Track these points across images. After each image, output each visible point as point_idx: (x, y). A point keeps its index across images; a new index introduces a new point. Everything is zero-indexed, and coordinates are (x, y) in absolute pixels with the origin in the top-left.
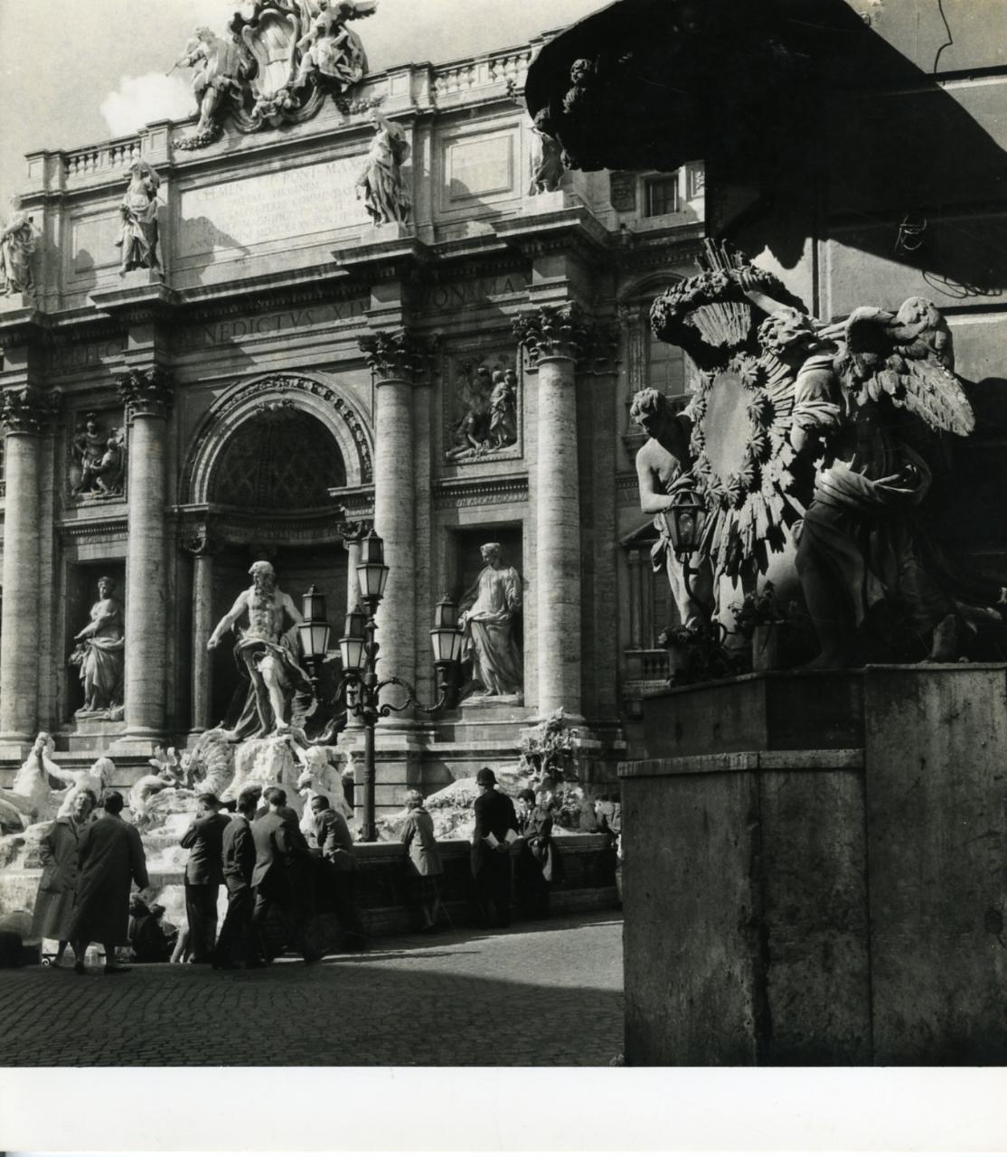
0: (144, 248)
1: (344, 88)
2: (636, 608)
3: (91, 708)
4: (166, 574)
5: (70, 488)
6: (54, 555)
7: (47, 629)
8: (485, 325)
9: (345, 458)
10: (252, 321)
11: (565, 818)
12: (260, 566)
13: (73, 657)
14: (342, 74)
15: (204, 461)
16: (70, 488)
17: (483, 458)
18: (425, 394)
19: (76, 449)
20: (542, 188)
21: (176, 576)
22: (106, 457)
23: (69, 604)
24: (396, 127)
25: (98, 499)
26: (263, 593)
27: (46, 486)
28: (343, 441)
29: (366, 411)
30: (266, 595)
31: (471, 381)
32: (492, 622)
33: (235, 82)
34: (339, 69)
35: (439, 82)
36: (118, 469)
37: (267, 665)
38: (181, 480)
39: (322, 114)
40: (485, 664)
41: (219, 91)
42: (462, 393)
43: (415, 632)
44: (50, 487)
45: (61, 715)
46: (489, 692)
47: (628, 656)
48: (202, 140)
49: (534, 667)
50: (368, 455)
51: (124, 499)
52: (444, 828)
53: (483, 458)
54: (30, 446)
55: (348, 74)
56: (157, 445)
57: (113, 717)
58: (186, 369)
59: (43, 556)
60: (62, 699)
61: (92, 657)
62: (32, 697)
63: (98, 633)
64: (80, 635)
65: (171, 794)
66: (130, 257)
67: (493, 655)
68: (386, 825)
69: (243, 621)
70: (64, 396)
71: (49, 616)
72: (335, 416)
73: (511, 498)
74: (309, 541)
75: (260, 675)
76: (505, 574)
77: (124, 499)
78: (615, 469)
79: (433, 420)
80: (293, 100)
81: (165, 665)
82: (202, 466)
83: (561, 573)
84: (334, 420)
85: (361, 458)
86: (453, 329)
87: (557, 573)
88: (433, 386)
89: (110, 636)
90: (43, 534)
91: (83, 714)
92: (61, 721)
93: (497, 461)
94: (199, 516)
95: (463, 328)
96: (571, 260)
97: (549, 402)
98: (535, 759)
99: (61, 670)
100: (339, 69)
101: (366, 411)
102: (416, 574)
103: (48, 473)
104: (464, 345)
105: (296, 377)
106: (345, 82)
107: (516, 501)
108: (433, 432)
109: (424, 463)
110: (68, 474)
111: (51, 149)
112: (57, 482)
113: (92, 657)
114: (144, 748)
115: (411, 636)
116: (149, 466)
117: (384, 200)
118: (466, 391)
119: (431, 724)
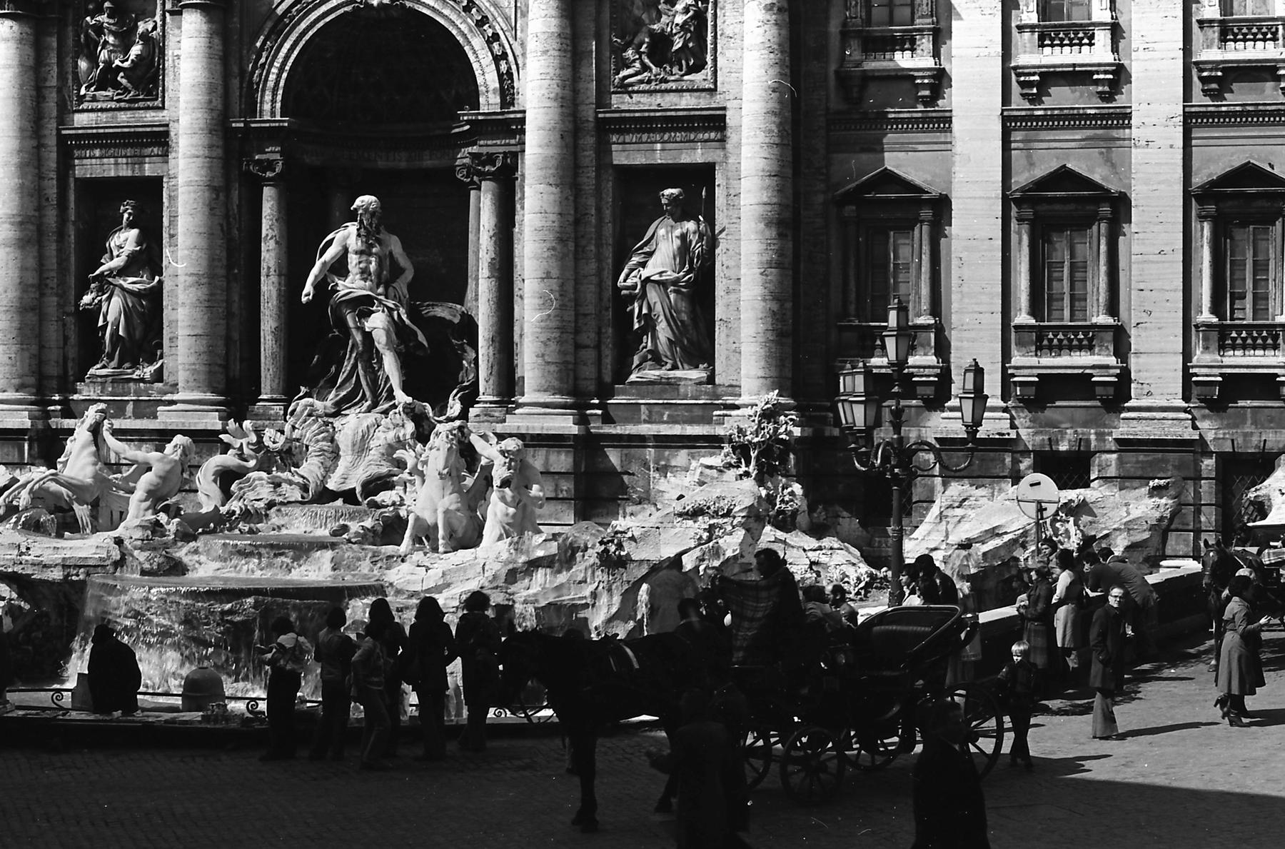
2: (852, 273)
3: (114, 364)
6: (58, 171)
7: (52, 262)
12: (365, 201)
13: (87, 299)
15: (277, 64)
17: (664, 86)
21: (239, 206)
22: (136, 50)
25: (119, 101)
26: (369, 235)
27: (46, 80)
28: (475, 52)
29: (507, 19)
30: (369, 235)
32: (675, 282)
37: (377, 322)
40: (663, 331)
43: (576, 291)
44: (53, 82)
46: (669, 366)
47: (842, 329)
51: (158, 103)
52: (701, 538)
53: (664, 86)
54: (28, 30)
56: (216, 41)
57: (147, 376)
59: (43, 170)
60: (72, 353)
61: (117, 302)
63: (123, 272)
64: (97, 272)
65: (261, 479)
68: (629, 534)
69: (339, 268)
71: (54, 246)
72: (465, 21)
73: (700, 136)
74: (403, 165)
75: (368, 337)
76: (690, 226)
78: (827, 109)
81: (229, 315)
82: (274, 70)
83: (774, 234)
85: (500, 75)
87: (773, 233)
90: (43, 141)
93: (682, 91)
94: (272, 134)
97: (761, 30)
98: (742, 451)
101: (507, 19)
102: (577, 222)
103: (49, 65)
107: (706, 141)
112: (62, 76)
113: (117, 302)
114: (211, 421)
115: (572, 296)
116: (211, 71)
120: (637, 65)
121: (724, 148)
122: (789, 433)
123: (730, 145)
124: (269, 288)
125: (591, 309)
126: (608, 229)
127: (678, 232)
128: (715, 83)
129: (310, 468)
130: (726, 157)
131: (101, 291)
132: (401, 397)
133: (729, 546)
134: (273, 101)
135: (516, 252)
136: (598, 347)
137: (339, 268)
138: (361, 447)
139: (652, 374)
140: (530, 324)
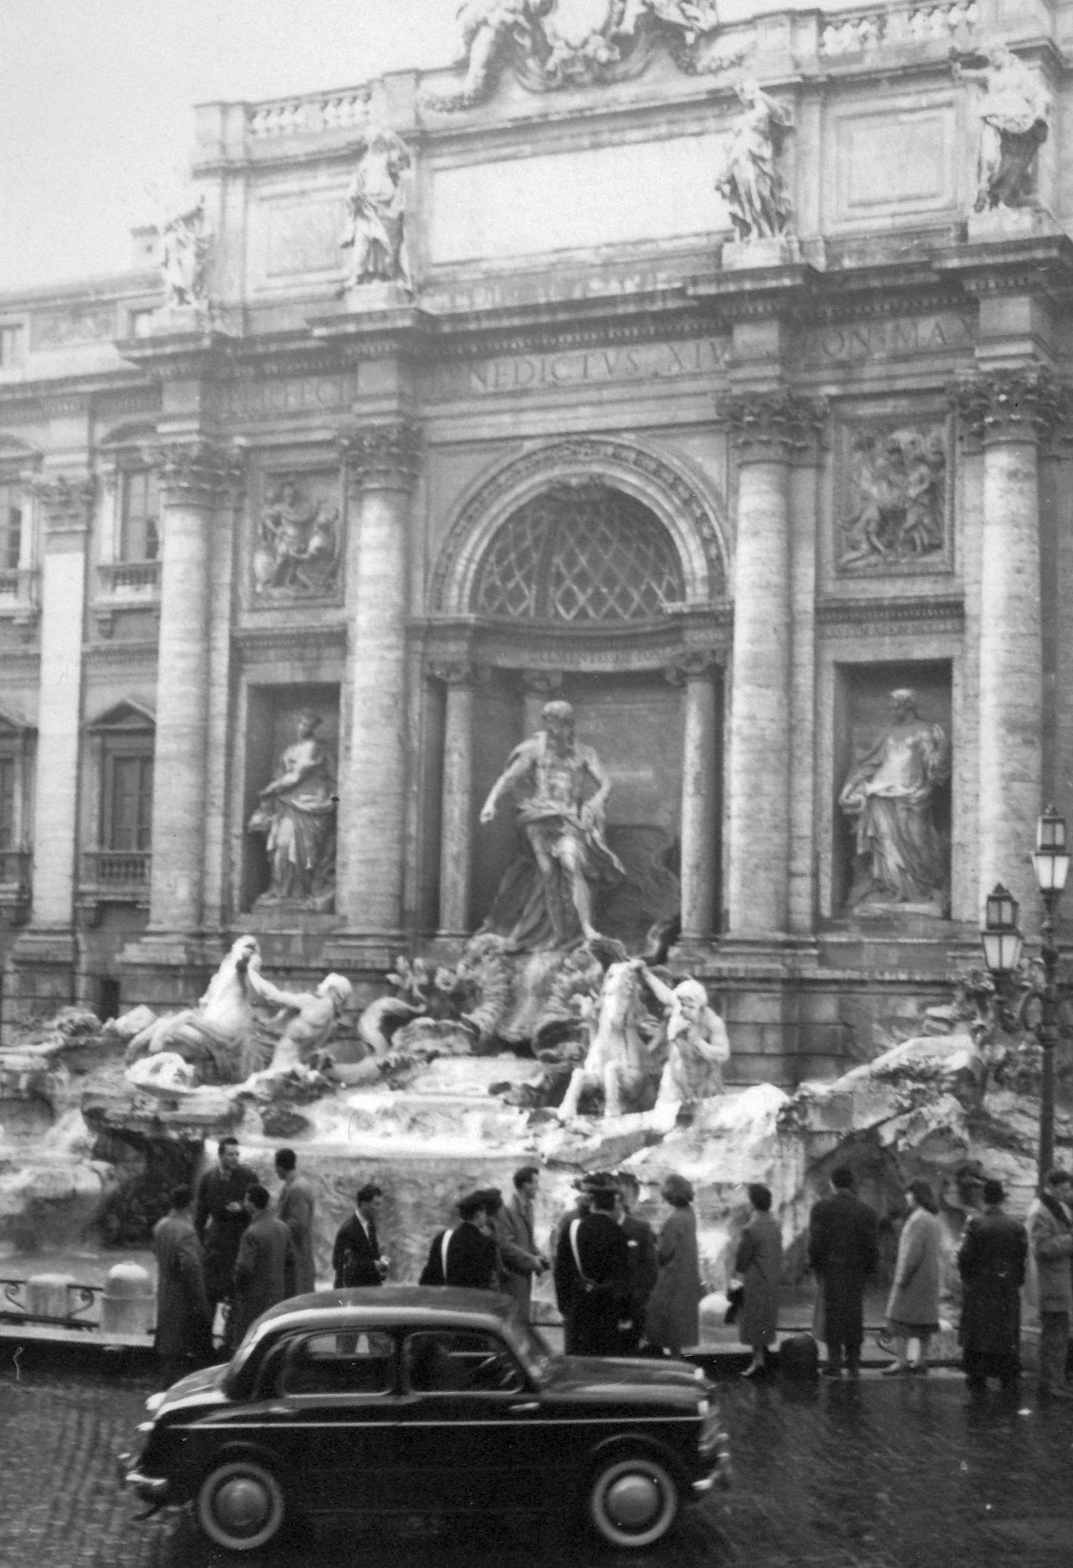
0: (386, 252)
1: (690, 37)
4: (405, 713)
5: (254, 580)
7: (218, 779)
8: (900, 385)
9: (685, 559)
10: (543, 362)
11: (1023, 1081)
14: (688, 18)
16: (254, 580)
18: (806, 479)
19: (265, 526)
20: (994, 203)
21: (421, 715)
23: (249, 745)
24: (777, 102)
29: (718, 496)
31: (872, 460)
32: (905, 799)
33: (521, 19)
34: (683, 11)
35: (829, 33)
36: (331, 554)
37: (569, 849)
38: (431, 577)
39: (649, 76)
41: (498, 32)
42: (860, 475)
44: (226, 577)
45: (236, 902)
48: (469, 98)
49: (969, 866)
50: (719, 558)
51: (336, 600)
55: (696, 19)
57: (319, 907)
58: (441, 423)
60: (237, 879)
62: (196, 875)
66: (364, 263)
67: (904, 844)
69: (527, 783)
70: (247, 451)
72: (668, 498)
77: (336, 600)
79: (818, 512)
80: (610, 48)
81: (403, 839)
84: (669, 508)
86: (854, 389)
88: (820, 467)
89: (314, 793)
91: (271, 902)
92: (236, 909)
95: (867, 388)
96: (1036, 301)
99: (237, 837)
100: (683, 11)
101: (718, 496)
102: (791, 730)
104: (867, 410)
105: (611, 443)
106: (691, 29)
108: (818, 534)
109: (805, 574)
110: (252, 562)
111: (231, 97)
112: (236, 573)
117: (758, 204)
118: (866, 473)
119: (813, 939)
120: (865, 546)
121: (961, 641)
122: (1032, 979)
123: (969, 638)
124: (455, 806)
125: (806, 830)
126: (828, 739)
127: (910, 740)
128: (952, 565)
129: (483, 1016)
130: (964, 651)
131: (272, 810)
132: (591, 934)
133: (933, 1115)
134: (460, 596)
135: (726, 764)
136: (815, 875)
137: (527, 783)
138: (543, 991)
139: (877, 907)
140: (92, 862)
